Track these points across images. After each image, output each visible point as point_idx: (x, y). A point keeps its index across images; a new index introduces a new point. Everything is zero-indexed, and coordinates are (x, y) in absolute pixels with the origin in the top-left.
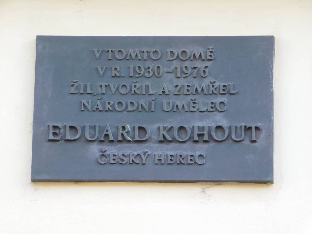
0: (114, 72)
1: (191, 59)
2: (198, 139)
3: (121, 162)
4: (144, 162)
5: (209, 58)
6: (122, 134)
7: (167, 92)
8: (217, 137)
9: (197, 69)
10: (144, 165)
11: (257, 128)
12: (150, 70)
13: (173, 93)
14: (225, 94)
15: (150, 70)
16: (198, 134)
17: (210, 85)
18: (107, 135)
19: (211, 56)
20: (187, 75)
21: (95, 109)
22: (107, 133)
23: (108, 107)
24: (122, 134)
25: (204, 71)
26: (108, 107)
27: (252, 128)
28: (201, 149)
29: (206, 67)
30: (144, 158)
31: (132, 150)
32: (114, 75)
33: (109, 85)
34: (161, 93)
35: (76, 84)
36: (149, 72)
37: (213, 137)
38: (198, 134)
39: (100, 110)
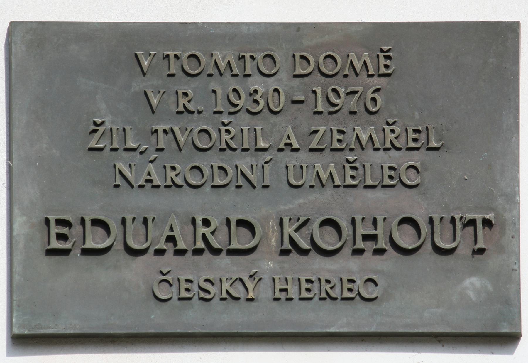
0: (183, 101)
1: (345, 73)
2: (364, 245)
3: (202, 295)
4: (251, 295)
5: (383, 70)
6: (204, 235)
7: (296, 146)
8: (409, 179)
9: (359, 94)
10: (253, 304)
11: (487, 223)
12: (257, 97)
13: (85, 215)
14: (418, 149)
15: (257, 97)
16: (363, 235)
17: (386, 129)
18: (171, 239)
19: (386, 66)
20: (337, 108)
21: (282, 146)
22: (171, 233)
23: (171, 178)
24: (204, 235)
25: (374, 99)
26: (171, 178)
27: (477, 222)
28: (371, 264)
29: (377, 90)
30: (250, 285)
31: (225, 267)
32: (181, 108)
33: (172, 130)
34: (283, 147)
35: (101, 129)
36: (256, 102)
37: (394, 239)
38: (363, 235)
39: (155, 183)
